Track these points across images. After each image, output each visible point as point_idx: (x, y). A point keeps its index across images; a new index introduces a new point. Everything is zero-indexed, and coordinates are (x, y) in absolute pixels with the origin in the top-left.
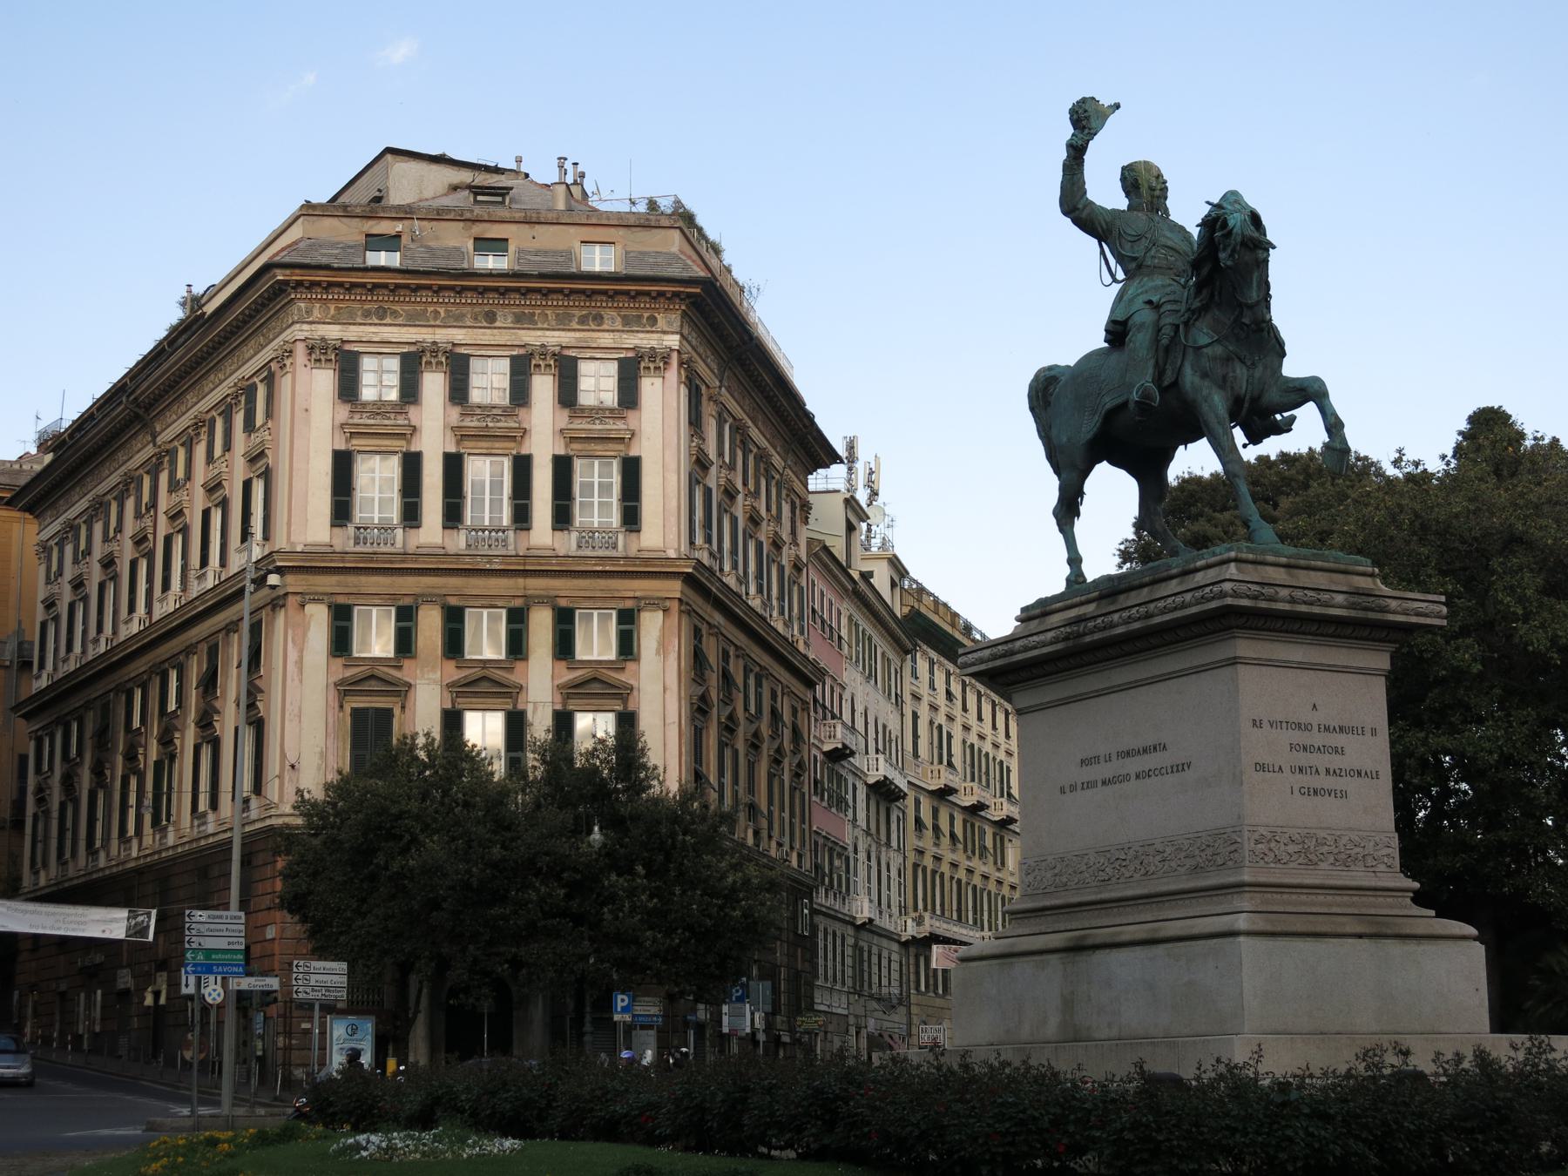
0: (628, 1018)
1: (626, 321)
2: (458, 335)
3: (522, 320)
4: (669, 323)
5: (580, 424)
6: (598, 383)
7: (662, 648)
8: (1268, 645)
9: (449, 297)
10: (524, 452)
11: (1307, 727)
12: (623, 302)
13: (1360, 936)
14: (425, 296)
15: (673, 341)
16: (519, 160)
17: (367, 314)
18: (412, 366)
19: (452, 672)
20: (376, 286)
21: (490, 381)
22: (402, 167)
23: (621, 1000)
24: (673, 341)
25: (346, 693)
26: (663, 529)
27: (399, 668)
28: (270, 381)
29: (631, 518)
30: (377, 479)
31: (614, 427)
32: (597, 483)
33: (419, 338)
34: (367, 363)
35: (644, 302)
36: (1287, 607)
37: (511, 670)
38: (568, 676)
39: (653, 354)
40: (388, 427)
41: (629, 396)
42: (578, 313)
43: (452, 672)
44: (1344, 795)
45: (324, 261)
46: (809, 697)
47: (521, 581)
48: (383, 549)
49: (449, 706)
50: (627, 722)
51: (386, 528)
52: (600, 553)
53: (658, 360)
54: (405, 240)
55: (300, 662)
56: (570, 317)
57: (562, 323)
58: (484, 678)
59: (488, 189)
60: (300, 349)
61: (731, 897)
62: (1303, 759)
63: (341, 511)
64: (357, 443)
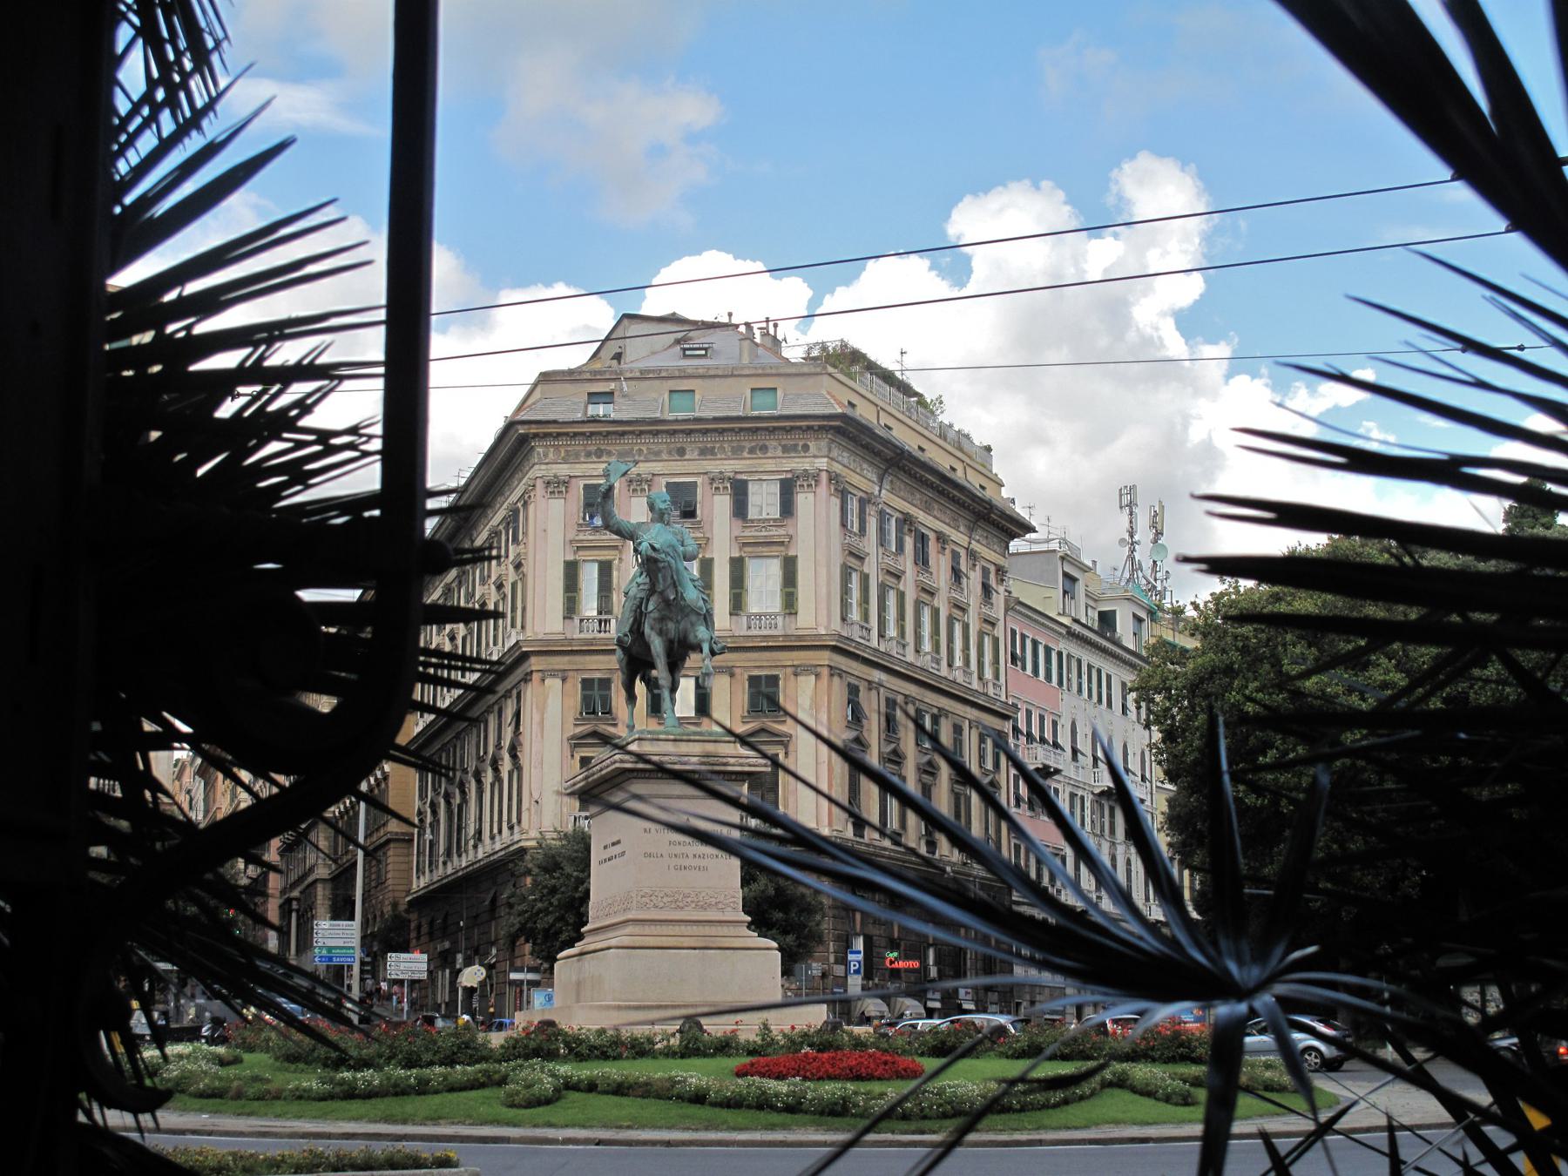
1: (785, 449)
14: (628, 440)
16: (730, 315)
17: (589, 455)
18: (788, 490)
20: (592, 434)
24: (822, 463)
25: (576, 745)
28: (525, 504)
29: (790, 604)
31: (776, 533)
32: (764, 580)
41: (787, 508)
42: (748, 445)
45: (551, 417)
46: (1007, 727)
53: (812, 478)
55: (542, 722)
56: (741, 449)
57: (737, 452)
60: (539, 483)
64: (582, 555)
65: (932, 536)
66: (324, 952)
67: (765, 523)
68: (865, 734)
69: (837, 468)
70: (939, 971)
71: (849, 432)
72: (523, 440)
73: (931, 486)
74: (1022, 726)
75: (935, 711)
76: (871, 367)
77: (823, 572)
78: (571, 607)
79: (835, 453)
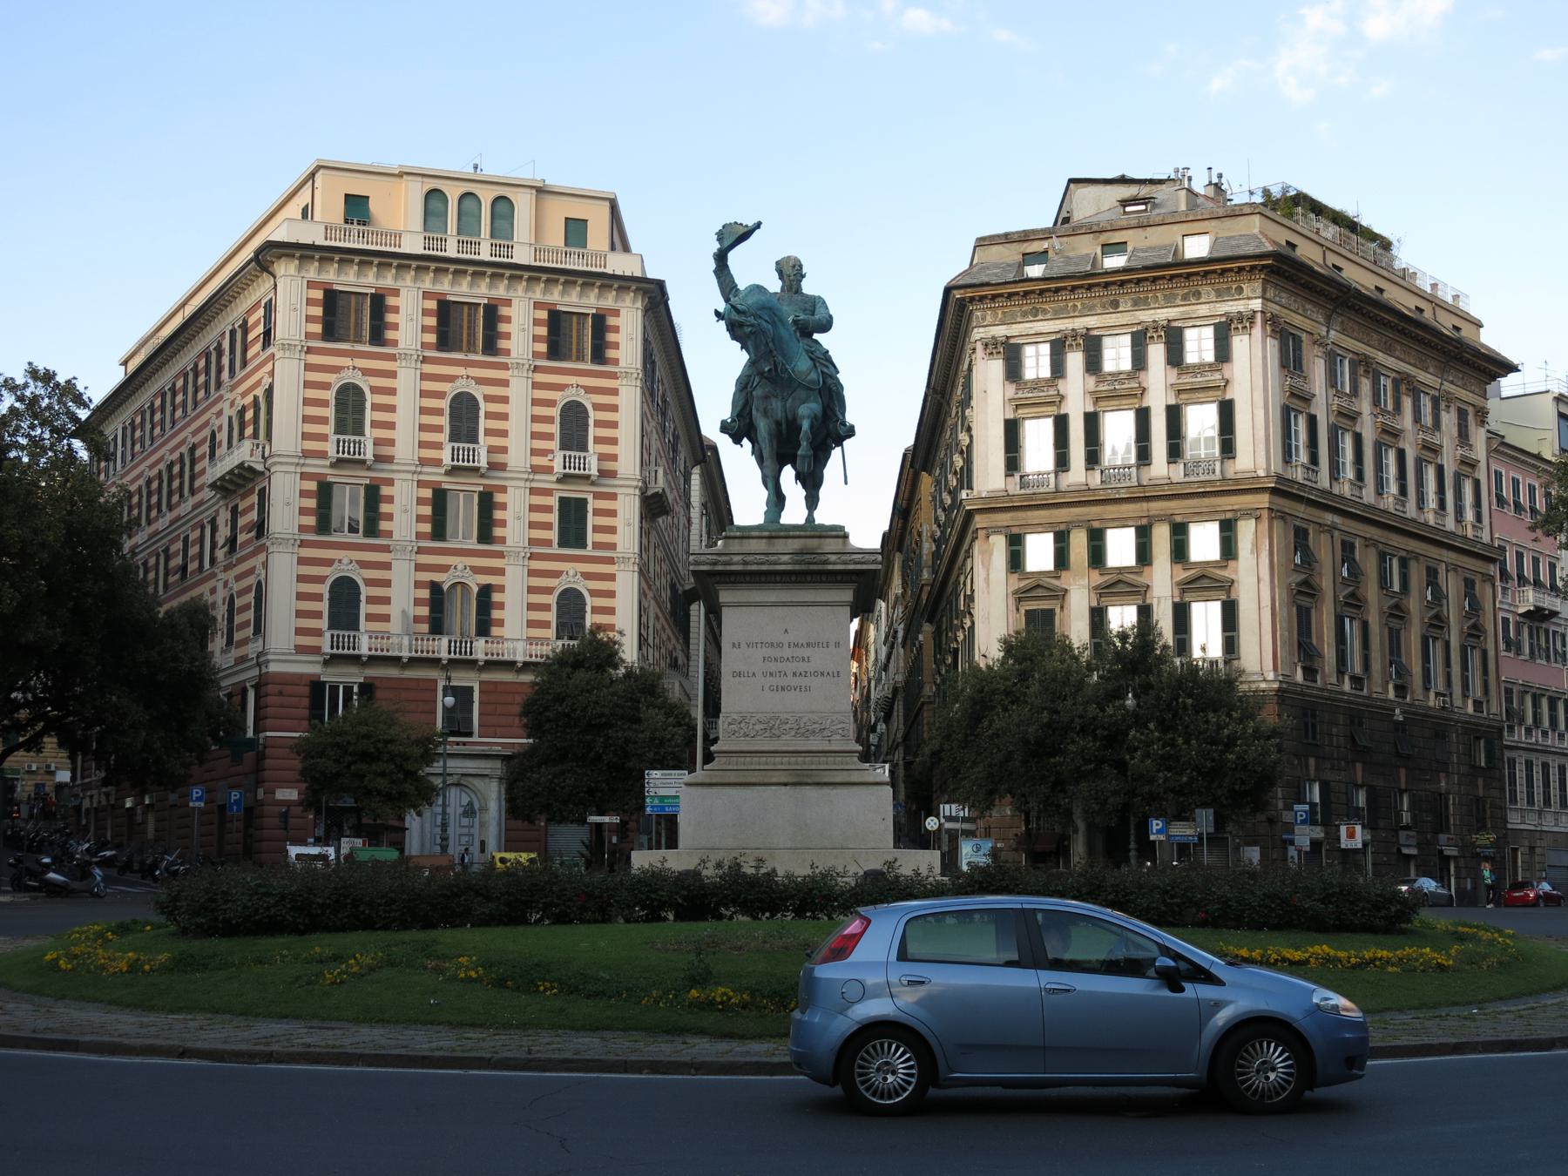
0: (1162, 837)
1: (1219, 293)
2: (1091, 321)
3: (1139, 304)
4: (1254, 291)
5: (1103, 387)
6: (1199, 345)
7: (1256, 549)
8: (746, 593)
9: (1081, 293)
10: (1228, 397)
11: (780, 645)
12: (1214, 278)
13: (786, 785)
14: (1064, 295)
15: (1256, 304)
17: (1024, 314)
18: (1059, 350)
19: (1097, 578)
21: (1117, 355)
22: (1081, 192)
23: (1156, 825)
24: (1256, 304)
25: (1020, 600)
26: (1255, 454)
27: (1058, 578)
29: (1228, 448)
30: (1118, 430)
33: (1063, 327)
34: (1029, 351)
35: (1231, 276)
36: (740, 568)
37: (1058, 578)
38: (1183, 575)
39: (1240, 317)
40: (1045, 398)
41: (1223, 352)
42: (1180, 292)
43: (1097, 578)
44: (807, 689)
45: (985, 279)
47: (1145, 505)
48: (1042, 490)
49: (1094, 604)
50: (1145, 612)
51: (1210, 461)
52: (1202, 478)
53: (1244, 321)
54: (1050, 254)
55: (987, 580)
56: (1174, 296)
57: (1169, 302)
58: (1119, 581)
59: (1140, 195)
60: (979, 347)
61: (1230, 743)
62: (773, 667)
63: (1013, 463)
65: (1470, 410)
66: (656, 801)
67: (1201, 368)
68: (1317, 579)
69: (1275, 309)
70: (1414, 817)
71: (1282, 270)
72: (962, 305)
73: (1388, 325)
74: (1511, 566)
75: (1404, 554)
76: (1317, 208)
77: (1260, 414)
78: (1013, 463)
79: (1270, 294)
